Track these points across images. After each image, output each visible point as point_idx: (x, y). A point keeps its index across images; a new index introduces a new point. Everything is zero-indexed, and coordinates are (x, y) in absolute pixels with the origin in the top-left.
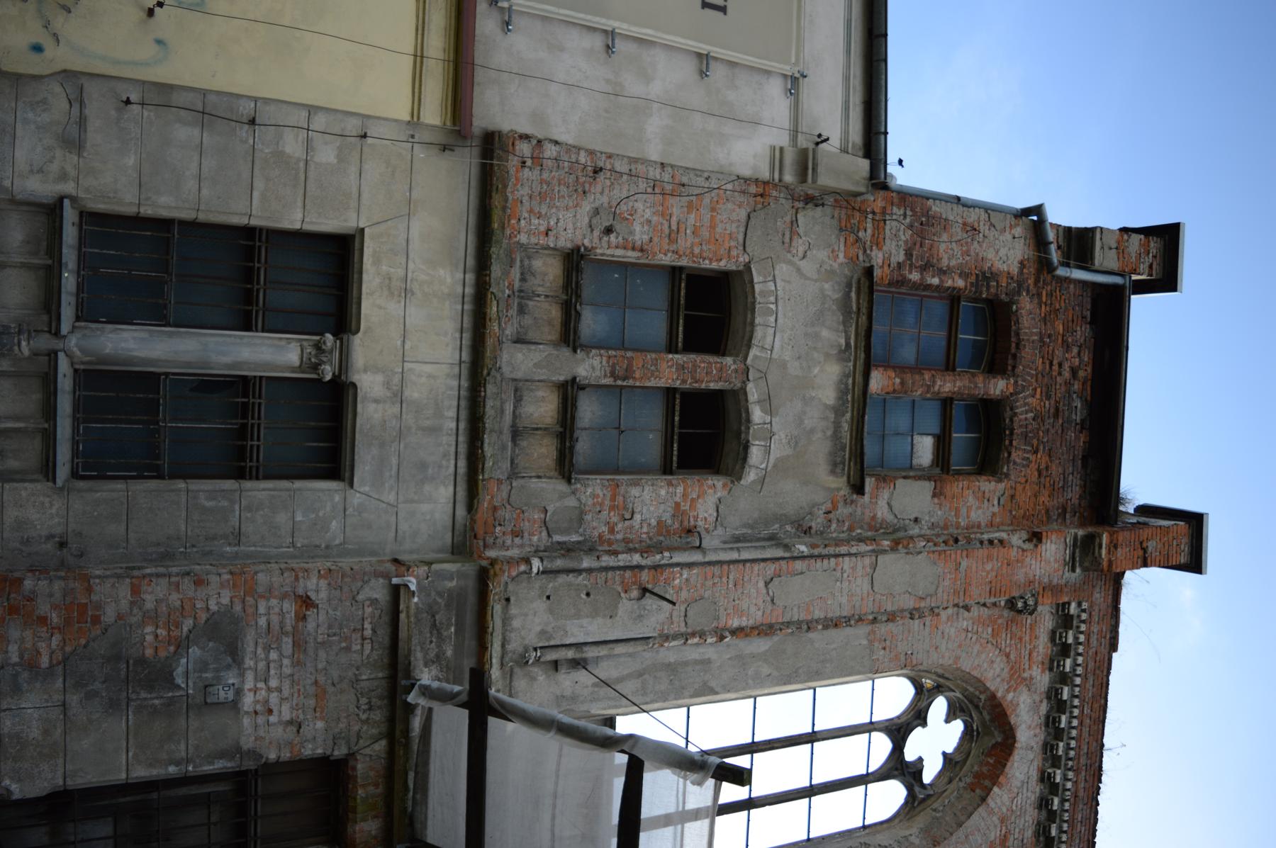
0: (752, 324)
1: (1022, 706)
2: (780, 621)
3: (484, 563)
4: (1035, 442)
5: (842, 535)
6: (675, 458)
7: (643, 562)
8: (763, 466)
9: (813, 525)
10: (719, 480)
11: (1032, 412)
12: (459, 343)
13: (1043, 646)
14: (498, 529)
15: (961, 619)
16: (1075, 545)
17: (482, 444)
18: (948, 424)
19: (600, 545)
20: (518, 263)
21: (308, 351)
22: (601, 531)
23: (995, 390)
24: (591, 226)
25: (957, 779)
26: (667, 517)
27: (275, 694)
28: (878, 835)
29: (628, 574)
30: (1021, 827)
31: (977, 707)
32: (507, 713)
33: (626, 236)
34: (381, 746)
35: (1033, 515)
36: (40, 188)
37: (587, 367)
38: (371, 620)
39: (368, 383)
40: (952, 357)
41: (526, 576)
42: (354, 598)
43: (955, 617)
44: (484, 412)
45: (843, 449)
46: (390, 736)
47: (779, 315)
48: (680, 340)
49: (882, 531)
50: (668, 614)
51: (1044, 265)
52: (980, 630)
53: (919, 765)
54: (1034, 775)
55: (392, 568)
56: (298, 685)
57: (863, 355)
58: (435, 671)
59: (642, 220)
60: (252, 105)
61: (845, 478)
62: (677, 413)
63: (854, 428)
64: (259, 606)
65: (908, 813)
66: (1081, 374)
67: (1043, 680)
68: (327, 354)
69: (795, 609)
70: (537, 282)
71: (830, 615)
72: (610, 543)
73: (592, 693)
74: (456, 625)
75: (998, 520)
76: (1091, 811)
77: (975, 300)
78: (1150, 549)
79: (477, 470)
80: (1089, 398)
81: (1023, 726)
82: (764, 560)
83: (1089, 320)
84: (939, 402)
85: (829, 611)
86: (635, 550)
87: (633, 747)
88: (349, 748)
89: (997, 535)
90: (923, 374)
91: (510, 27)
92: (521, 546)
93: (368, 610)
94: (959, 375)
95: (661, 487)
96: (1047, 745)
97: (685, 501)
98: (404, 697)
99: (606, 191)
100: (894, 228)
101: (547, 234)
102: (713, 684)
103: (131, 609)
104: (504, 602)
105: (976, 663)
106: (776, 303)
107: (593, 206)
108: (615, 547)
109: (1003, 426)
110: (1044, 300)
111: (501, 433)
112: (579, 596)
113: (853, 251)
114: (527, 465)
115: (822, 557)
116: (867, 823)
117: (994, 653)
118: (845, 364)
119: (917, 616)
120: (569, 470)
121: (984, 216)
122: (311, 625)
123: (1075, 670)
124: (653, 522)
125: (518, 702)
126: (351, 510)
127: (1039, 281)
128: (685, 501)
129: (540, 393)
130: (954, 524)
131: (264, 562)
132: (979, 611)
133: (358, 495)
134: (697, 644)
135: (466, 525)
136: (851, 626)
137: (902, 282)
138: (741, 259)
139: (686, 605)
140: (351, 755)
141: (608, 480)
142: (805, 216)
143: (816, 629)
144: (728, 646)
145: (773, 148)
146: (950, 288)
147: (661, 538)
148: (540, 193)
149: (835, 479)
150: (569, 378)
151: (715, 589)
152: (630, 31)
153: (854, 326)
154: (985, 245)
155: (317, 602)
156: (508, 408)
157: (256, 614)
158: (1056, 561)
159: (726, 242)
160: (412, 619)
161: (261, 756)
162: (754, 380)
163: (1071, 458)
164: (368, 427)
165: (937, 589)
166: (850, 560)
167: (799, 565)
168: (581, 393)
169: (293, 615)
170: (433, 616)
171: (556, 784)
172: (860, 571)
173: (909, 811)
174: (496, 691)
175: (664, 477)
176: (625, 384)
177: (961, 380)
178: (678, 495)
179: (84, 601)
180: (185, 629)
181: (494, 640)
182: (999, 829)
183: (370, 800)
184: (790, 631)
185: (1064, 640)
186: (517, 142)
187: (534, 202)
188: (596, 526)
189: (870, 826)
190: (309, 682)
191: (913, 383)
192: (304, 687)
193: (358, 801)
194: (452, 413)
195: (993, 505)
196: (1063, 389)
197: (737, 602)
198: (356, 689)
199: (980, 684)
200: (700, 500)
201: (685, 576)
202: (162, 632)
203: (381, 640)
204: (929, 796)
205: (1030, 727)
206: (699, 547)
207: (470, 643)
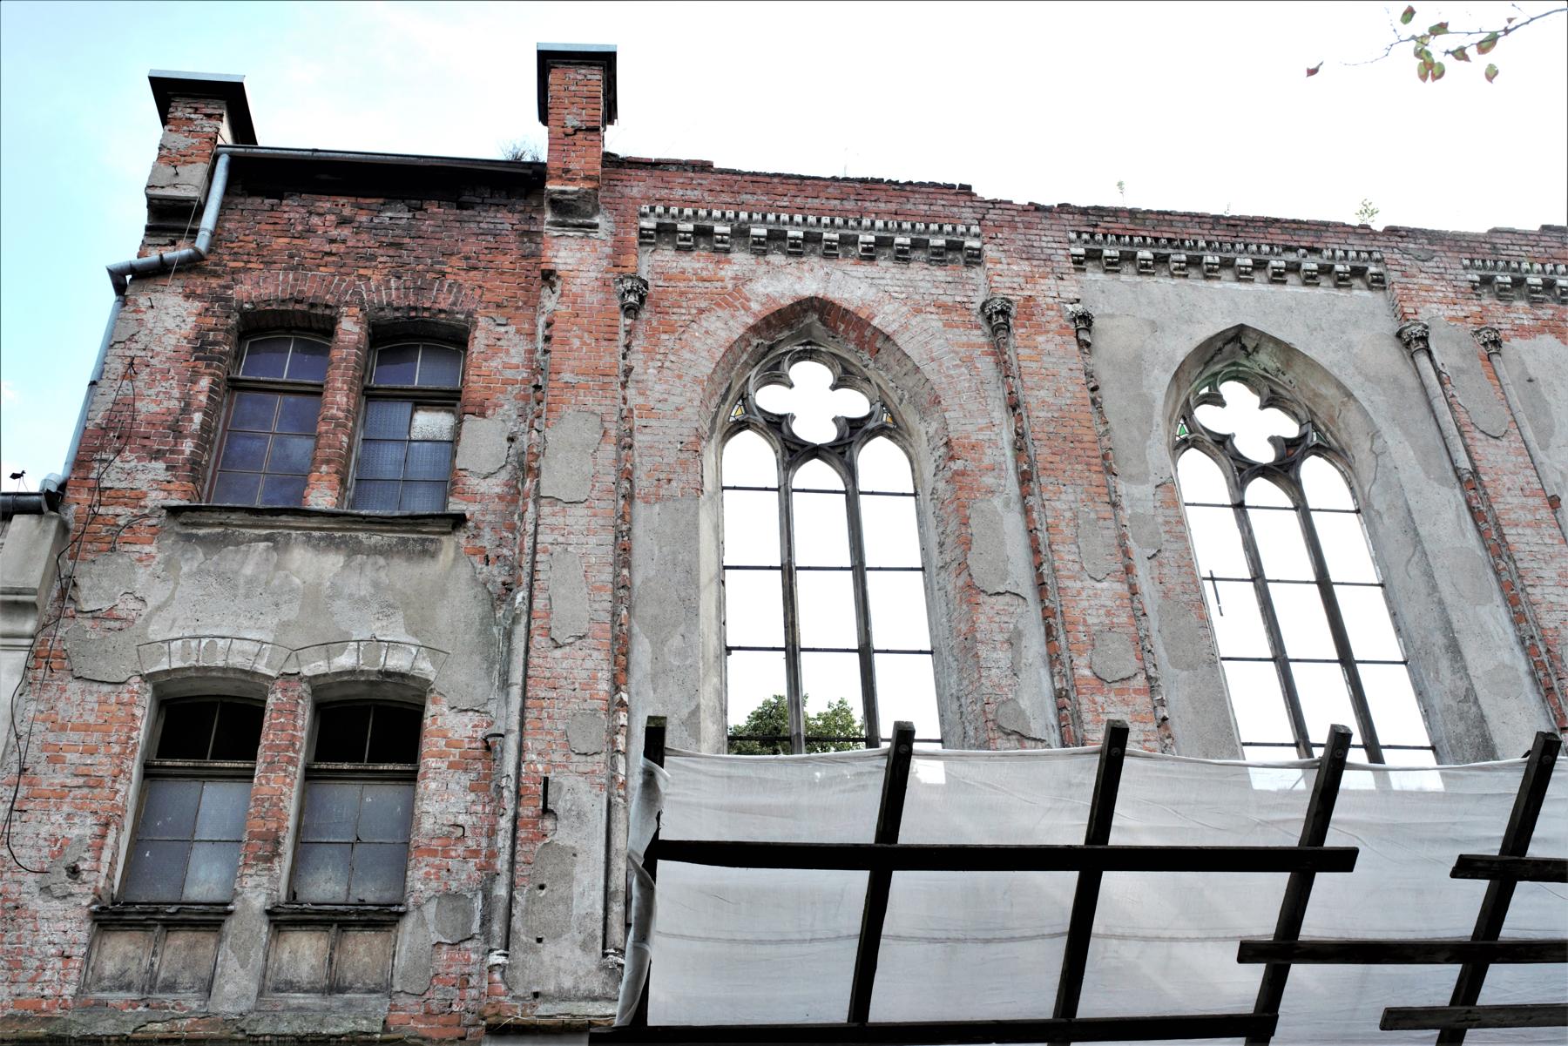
0: (224, 670)
1: (770, 290)
2: (608, 626)
4: (429, 276)
7: (510, 813)
8: (414, 650)
9: (500, 580)
11: (389, 281)
14: (455, 1008)
15: (645, 377)
16: (563, 225)
20: (105, 995)
24: (65, 897)
25: (865, 370)
26: (466, 779)
29: (522, 834)
30: (929, 285)
31: (771, 348)
33: (84, 847)
37: (254, 895)
40: (310, 389)
45: (405, 542)
47: (215, 634)
48: (242, 765)
51: (192, 265)
53: (842, 422)
54: (865, 269)
57: (283, 518)
59: (65, 826)
61: (444, 538)
66: (347, 212)
67: (741, 260)
69: (596, 606)
70: (133, 966)
75: (526, 326)
76: (919, 193)
77: (238, 357)
78: (576, 123)
79: (369, 1041)
80: (381, 201)
81: (797, 287)
83: (276, 201)
84: (369, 403)
87: (637, 855)
90: (320, 434)
95: (426, 788)
100: (119, 475)
101: (68, 957)
102: (685, 712)
104: (538, 1000)
105: (705, 354)
106: (199, 638)
107: (37, 895)
109: (404, 320)
110: (242, 264)
112: (541, 899)
113: (144, 534)
114: (378, 971)
118: (293, 541)
119: (629, 439)
121: (118, 350)
123: (730, 220)
127: (215, 272)
129: (285, 956)
130: (523, 386)
132: (638, 352)
134: (628, 737)
136: (630, 529)
137: (194, 464)
138: (136, 687)
139: (573, 754)
142: (87, 601)
146: (209, 398)
148: (10, 969)
149: (443, 552)
150: (266, 918)
151: (556, 716)
154: (158, 349)
156: (296, 1001)
158: (581, 250)
159: (108, 708)
163: (458, 225)
167: (539, 604)
168: (299, 898)
172: (559, 521)
177: (334, 380)
182: (929, 316)
184: (625, 612)
187: (21, 978)
188: (466, 874)
191: (330, 447)
195: (506, 332)
196: (364, 236)
197: (577, 686)
199: (736, 346)
200: (450, 735)
205: (799, 278)
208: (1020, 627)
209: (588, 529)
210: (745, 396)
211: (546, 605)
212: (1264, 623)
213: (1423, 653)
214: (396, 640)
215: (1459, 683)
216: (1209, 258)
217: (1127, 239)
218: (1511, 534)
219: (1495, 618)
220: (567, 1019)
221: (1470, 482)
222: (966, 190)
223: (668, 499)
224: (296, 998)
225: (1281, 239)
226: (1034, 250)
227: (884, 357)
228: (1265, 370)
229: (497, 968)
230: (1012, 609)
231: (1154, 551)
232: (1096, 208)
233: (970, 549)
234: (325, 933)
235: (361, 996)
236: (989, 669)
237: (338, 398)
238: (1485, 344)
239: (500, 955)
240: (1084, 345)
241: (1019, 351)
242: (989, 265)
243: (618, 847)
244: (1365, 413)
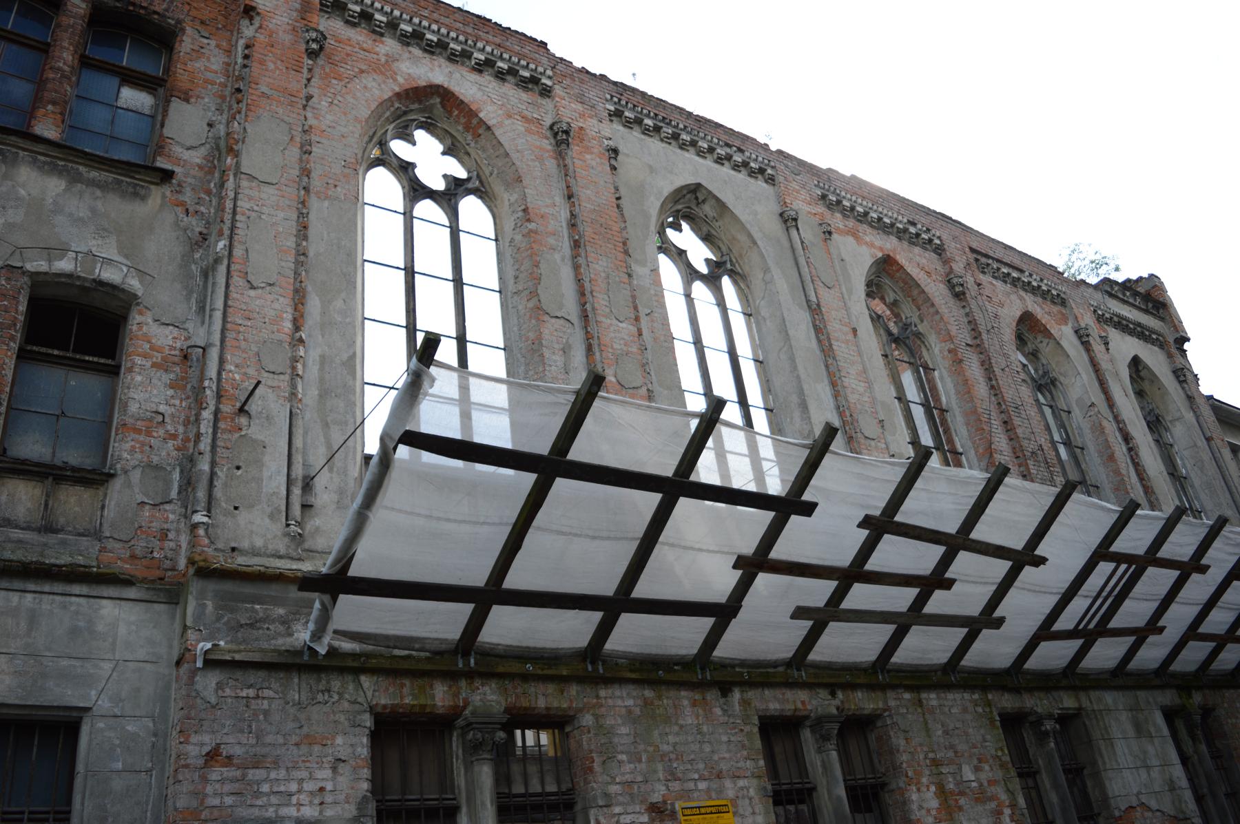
1: (410, 71)
2: (292, 281)
3: (191, 571)
5: (214, 202)
6: (102, 361)
7: (212, 408)
8: (125, 269)
9: (198, 229)
10: (134, 318)
13: (358, 36)
14: (156, 554)
15: (319, 107)
18: (111, 67)
19: (188, 450)
22: (172, 448)
23: (80, 8)
25: (467, 147)
26: (167, 378)
27: (305, 785)
28: (505, 229)
29: (222, 425)
30: (517, 101)
31: (405, 113)
32: (346, 556)
34: (365, 680)
35: (226, 8)
38: (239, 689)
41: (210, 529)
42: (213, 707)
43: (316, 111)
44: (17, 562)
45: (119, 182)
46: (357, 671)
49: (216, 162)
50: (268, 390)
52: (332, 91)
53: (450, 178)
54: (474, 77)
55: (185, 667)
56: (298, 762)
57: (13, 138)
58: (297, 627)
61: (152, 187)
62: (50, 351)
63: (96, 165)
64: (213, 804)
65: (490, 199)
67: (389, 45)
69: (283, 264)
71: (295, 232)
72: (187, 440)
73: (339, 474)
74: (253, 603)
75: (224, 44)
81: (430, 75)
82: (227, 286)
85: (289, 231)
86: (198, 416)
87: (391, 438)
88: (365, 711)
89: (240, 49)
90: (47, 79)
92: (178, 531)
93: (228, 692)
94: (55, 40)
95: (132, 379)
96: (542, 93)
97: (151, 357)
98: (320, 658)
102: (345, 356)
104: (235, 553)
105: (363, 102)
108: (191, 436)
111: (45, 545)
115: (233, 228)
116: (493, 237)
117: (357, 84)
119: (308, 147)
120: (99, 474)
122: (238, 751)
123: (386, 13)
124: (170, 392)
125: (337, 544)
126: (116, 710)
128: (151, 357)
131: (165, 802)
133: (100, 702)
134: (304, 366)
135: (148, 589)
136: (308, 213)
139: (263, 371)
140: (371, 709)
141: (117, 435)
143: (306, 248)
144: (310, 336)
147: (189, 386)
151: (250, 340)
155: (213, 745)
156: (16, 535)
157: (220, 807)
160: (242, 647)
161: (365, 797)
162: (23, 262)
164: (20, 691)
165: (285, 122)
166: (241, 200)
167: (238, 252)
168: (9, 453)
169: (225, 769)
170: (242, 626)
171: (419, 515)
172: (254, 193)
173: (488, 197)
174: (324, 567)
175: (122, 375)
176: (5, 404)
178: (144, 363)
181: (273, 565)
182: (516, 121)
183: (416, 691)
184: (303, 273)
185: (356, 15)
188: (167, 452)
189: (496, 235)
190: (295, 751)
191: (56, 91)
192: (300, 756)
193: (415, 702)
194: (15, 598)
195: (208, 44)
197: (267, 320)
198: (307, 705)
200: (153, 341)
201: (233, 368)
203: (260, 679)
204: (478, 176)
205: (431, 69)
206: (204, 349)
207: (274, 590)
208: (570, 342)
209: (277, 205)
210: (383, 142)
211: (243, 255)
212: (700, 371)
213: (784, 406)
214: (109, 257)
215: (805, 426)
216: (684, 136)
217: (640, 109)
218: (835, 345)
219: (824, 391)
220: (262, 569)
221: (815, 310)
222: (543, 45)
223: (335, 200)
224: (16, 533)
225: (724, 137)
226: (585, 98)
227: (482, 141)
228: (706, 216)
229: (201, 525)
230: (565, 329)
231: (649, 311)
232: (622, 83)
233: (539, 284)
234: (39, 484)
235: (74, 537)
236: (551, 366)
237: (65, 55)
238: (824, 232)
239: (204, 515)
240: (614, 168)
241: (575, 160)
242: (557, 99)
243: (298, 446)
244: (763, 256)
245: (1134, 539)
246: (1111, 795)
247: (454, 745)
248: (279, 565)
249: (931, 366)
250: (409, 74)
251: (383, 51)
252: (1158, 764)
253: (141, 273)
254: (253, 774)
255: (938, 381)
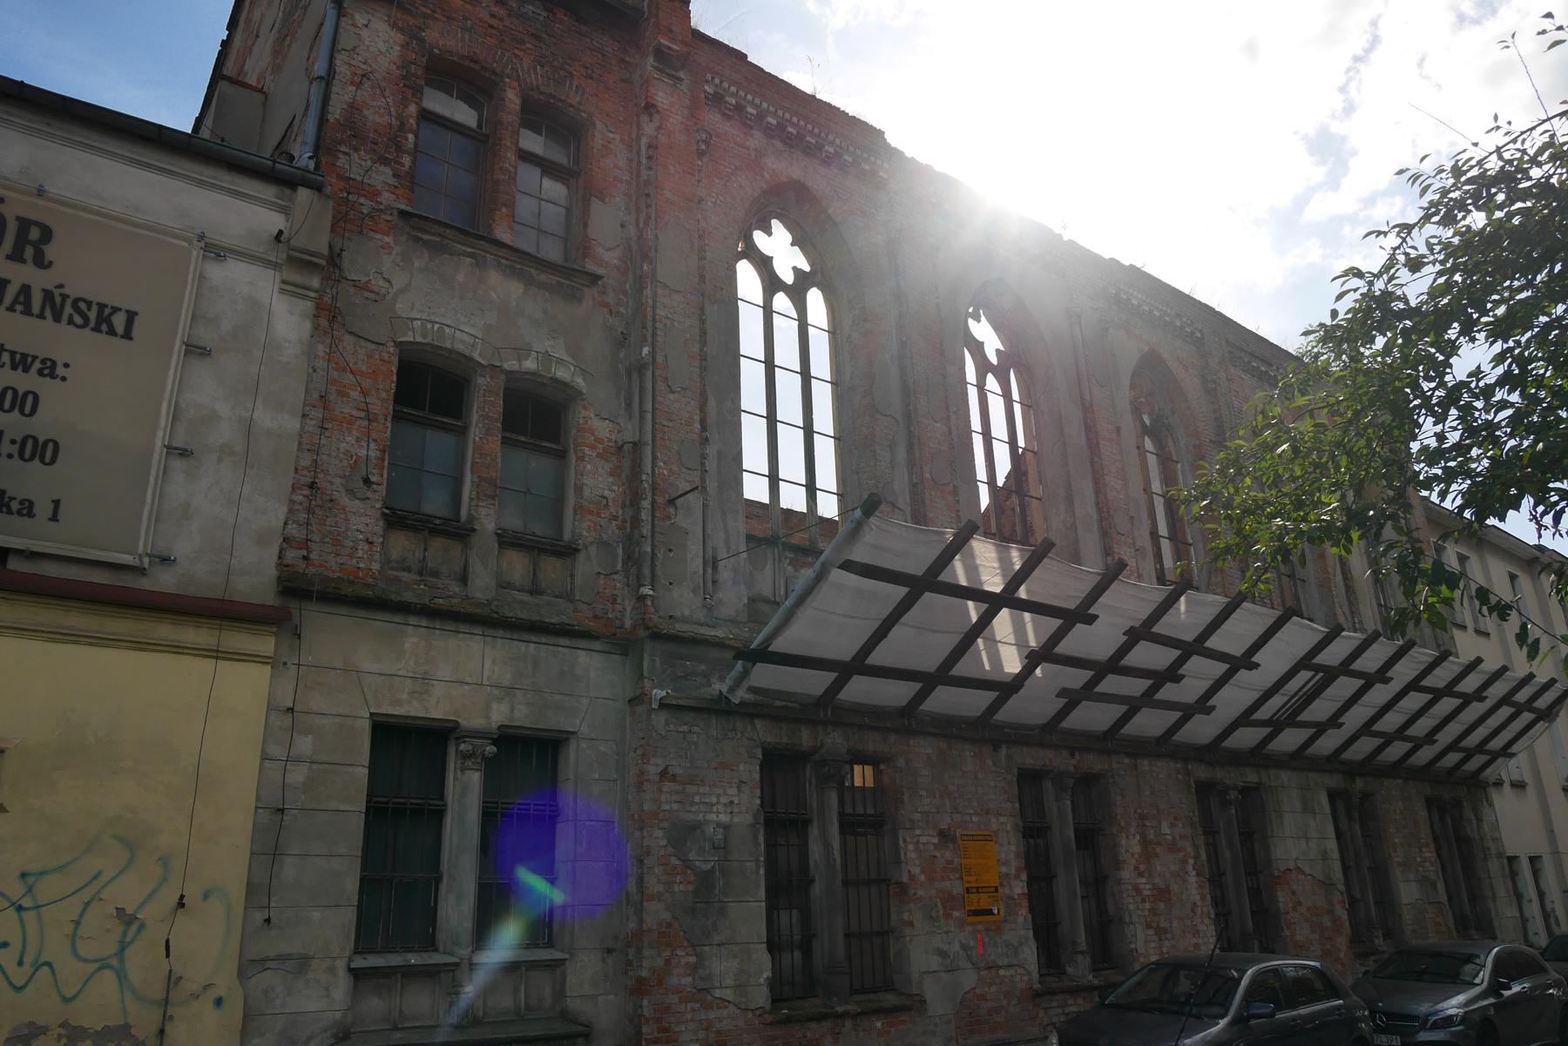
0: (451, 351)
1: (775, 166)
7: (650, 499)
8: (572, 368)
9: (620, 330)
10: (579, 412)
12: (467, 635)
17: (552, 624)
21: (470, 764)
22: (615, 528)
24: (364, 499)
26: (608, 467)
36: (341, 987)
39: (499, 715)
46: (752, 716)
49: (629, 263)
57: (482, 242)
60: (260, 811)
61: (585, 289)
67: (757, 140)
68: (475, 750)
72: (624, 521)
91: (172, 558)
95: (585, 468)
98: (732, 705)
99: (329, 478)
101: (372, 543)
103: (663, 901)
106: (434, 322)
107: (344, 495)
115: (654, 335)
122: (678, 771)
135: (607, 643)
145: (282, 291)
147: (624, 474)
152: (166, 426)
153: (455, 244)
161: (758, 810)
167: (659, 359)
178: (591, 453)
179: (656, 933)
180: (677, 862)
186: (285, 562)
194: (523, 646)
200: (596, 434)
202: (678, 879)
215: (1068, 519)
245: (1333, 655)
246: (1273, 858)
247: (808, 775)
248: (702, 631)
249: (1175, 458)
250: (774, 170)
251: (752, 146)
252: (1317, 836)
253: (584, 372)
254: (690, 789)
255: (1180, 473)
